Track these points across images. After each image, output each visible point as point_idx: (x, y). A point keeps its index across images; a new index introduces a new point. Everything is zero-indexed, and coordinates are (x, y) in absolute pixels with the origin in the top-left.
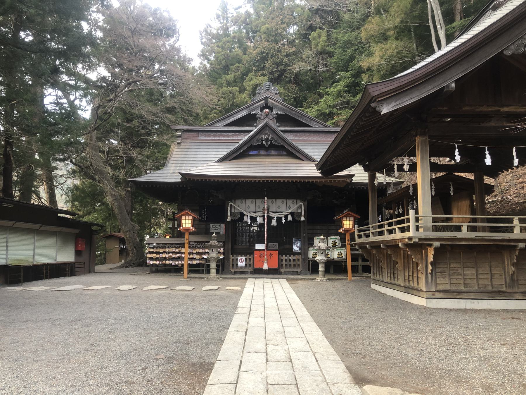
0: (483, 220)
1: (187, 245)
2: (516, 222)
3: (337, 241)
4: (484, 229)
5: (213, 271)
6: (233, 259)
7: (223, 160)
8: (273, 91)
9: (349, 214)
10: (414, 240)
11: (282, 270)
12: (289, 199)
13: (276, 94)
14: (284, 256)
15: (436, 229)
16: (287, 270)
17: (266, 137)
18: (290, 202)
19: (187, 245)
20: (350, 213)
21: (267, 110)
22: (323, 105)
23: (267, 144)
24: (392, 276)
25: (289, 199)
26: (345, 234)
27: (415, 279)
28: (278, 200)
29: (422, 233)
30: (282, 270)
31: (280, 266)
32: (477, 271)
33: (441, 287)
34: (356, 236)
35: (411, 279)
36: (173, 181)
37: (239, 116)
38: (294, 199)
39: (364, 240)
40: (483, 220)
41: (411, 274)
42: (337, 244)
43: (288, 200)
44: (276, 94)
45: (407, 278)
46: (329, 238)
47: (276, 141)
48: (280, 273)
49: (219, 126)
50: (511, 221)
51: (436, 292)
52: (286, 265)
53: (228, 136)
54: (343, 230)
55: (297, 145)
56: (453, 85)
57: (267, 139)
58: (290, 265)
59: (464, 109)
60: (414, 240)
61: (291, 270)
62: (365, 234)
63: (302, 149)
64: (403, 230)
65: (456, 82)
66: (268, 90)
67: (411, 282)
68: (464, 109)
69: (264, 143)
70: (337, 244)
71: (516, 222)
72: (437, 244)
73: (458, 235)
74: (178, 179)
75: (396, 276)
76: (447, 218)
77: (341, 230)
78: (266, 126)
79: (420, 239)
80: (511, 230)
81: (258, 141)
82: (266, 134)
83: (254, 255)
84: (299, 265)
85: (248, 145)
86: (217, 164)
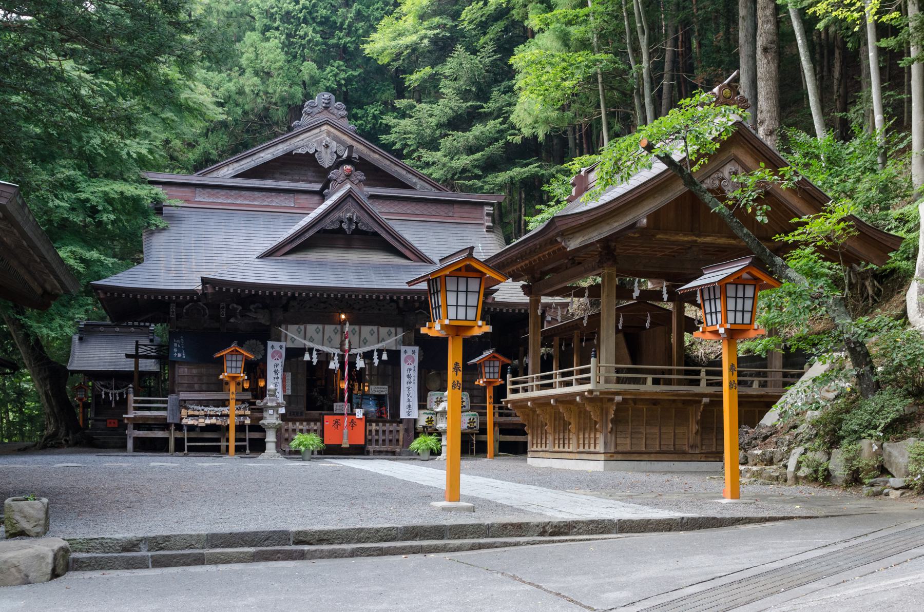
0: (679, 372)
1: (232, 402)
2: (703, 374)
4: (680, 382)
5: (271, 447)
7: (269, 255)
8: (336, 111)
10: (595, 393)
11: (371, 448)
13: (342, 117)
14: (374, 424)
15: (619, 381)
16: (378, 448)
17: (349, 215)
18: (384, 330)
19: (232, 402)
20: (496, 355)
21: (348, 167)
23: (349, 228)
24: (561, 442)
26: (485, 388)
27: (592, 441)
29: (603, 386)
30: (371, 448)
31: (368, 441)
32: (660, 429)
33: (620, 449)
34: (508, 391)
35: (587, 442)
36: (174, 288)
37: (267, 156)
39: (521, 395)
40: (679, 372)
41: (587, 436)
43: (381, 328)
44: (342, 117)
45: (581, 442)
47: (366, 225)
48: (368, 453)
49: (225, 173)
50: (698, 373)
51: (615, 453)
52: (384, 441)
55: (390, 223)
56: (645, 221)
57: (350, 219)
58: (377, 441)
59: (658, 236)
60: (595, 393)
61: (383, 448)
62: (523, 388)
63: (401, 233)
64: (581, 382)
65: (648, 217)
66: (326, 108)
67: (587, 446)
68: (658, 236)
69: (345, 226)
71: (703, 374)
72: (618, 398)
73: (642, 388)
74: (197, 286)
75: (566, 442)
78: (349, 195)
79: (602, 392)
80: (697, 383)
81: (332, 223)
82: (348, 211)
83: (323, 425)
84: (398, 440)
85: (315, 230)
86: (261, 263)
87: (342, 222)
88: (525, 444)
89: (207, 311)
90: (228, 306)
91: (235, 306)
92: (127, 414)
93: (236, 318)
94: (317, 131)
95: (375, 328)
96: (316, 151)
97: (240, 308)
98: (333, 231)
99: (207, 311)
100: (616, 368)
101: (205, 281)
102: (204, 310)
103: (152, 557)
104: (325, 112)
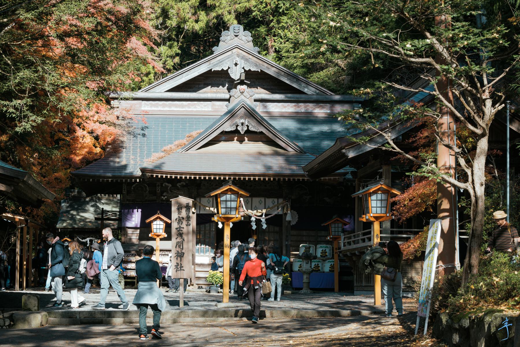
3: (327, 250)
6: (286, 245)
9: (338, 220)
12: (268, 198)
20: (339, 219)
22: (401, 49)
23: (242, 130)
25: (269, 197)
28: (72, 291)
38: (275, 198)
42: (327, 254)
43: (267, 199)
46: (318, 246)
53: (183, 106)
54: (330, 238)
62: (367, 238)
69: (239, 128)
70: (327, 254)
76: (399, 231)
77: (329, 238)
87: (237, 126)
88: (352, 282)
89: (148, 188)
90: (162, 184)
91: (167, 184)
92: (452, 192)
93: (168, 193)
94: (230, 53)
95: (263, 199)
96: (229, 68)
97: (170, 185)
98: (231, 132)
99: (148, 188)
100: (391, 231)
101: (143, 170)
102: (146, 187)
103: (44, 290)
104: (236, 38)
